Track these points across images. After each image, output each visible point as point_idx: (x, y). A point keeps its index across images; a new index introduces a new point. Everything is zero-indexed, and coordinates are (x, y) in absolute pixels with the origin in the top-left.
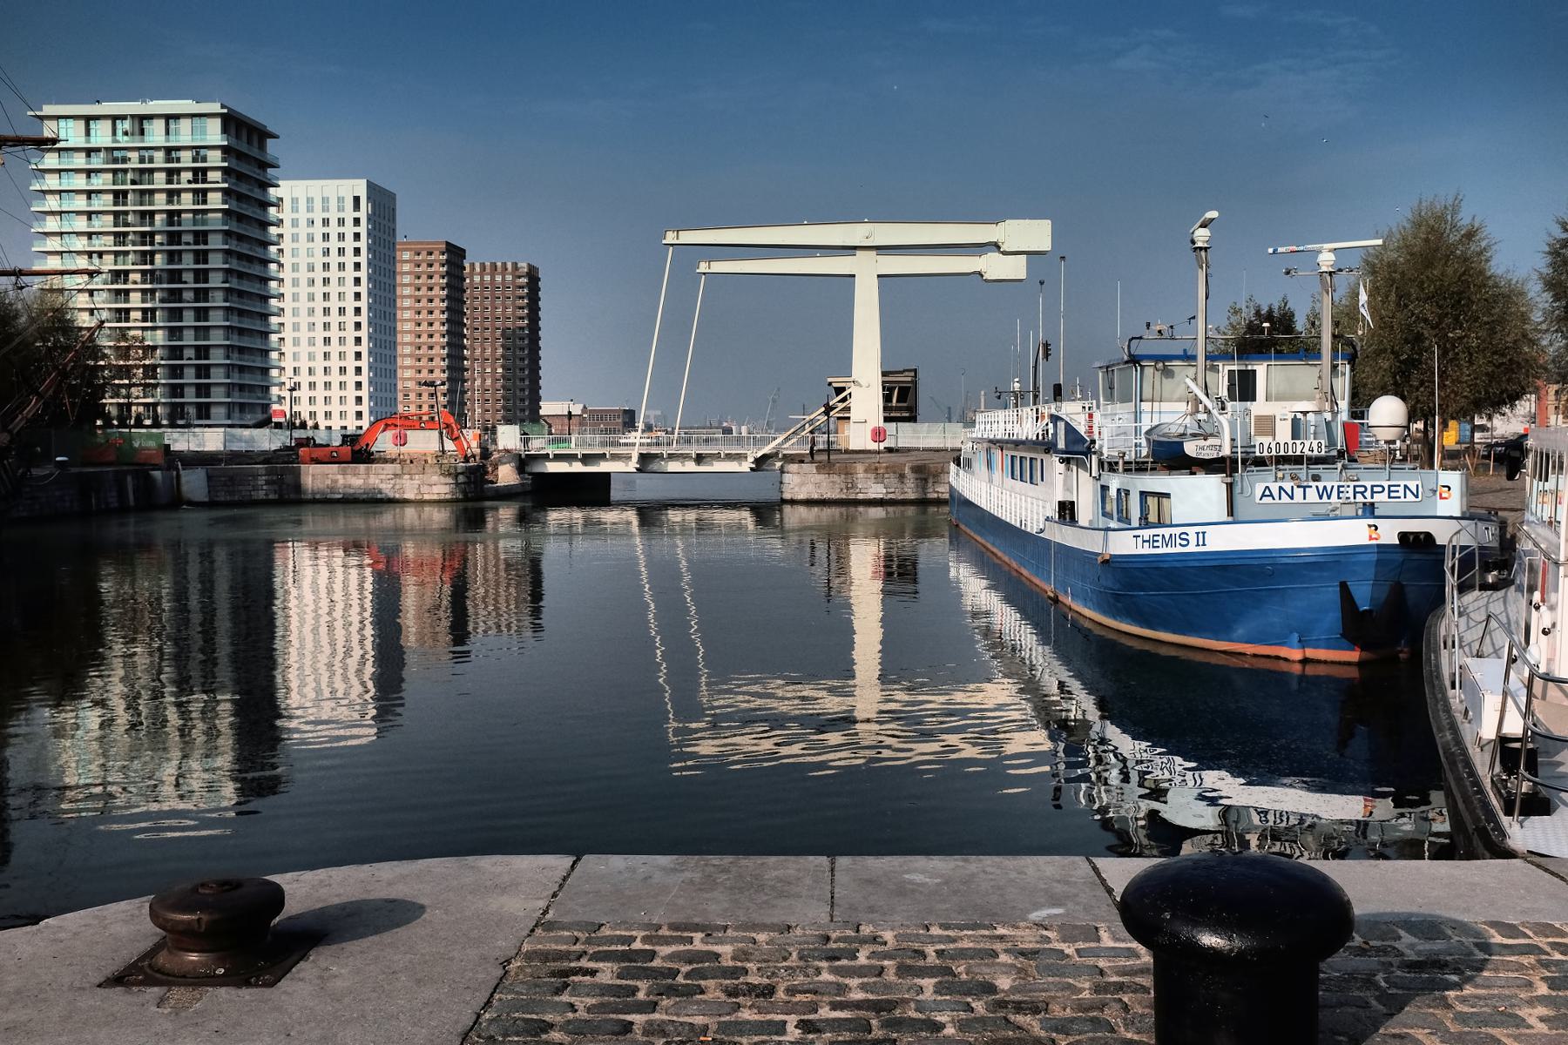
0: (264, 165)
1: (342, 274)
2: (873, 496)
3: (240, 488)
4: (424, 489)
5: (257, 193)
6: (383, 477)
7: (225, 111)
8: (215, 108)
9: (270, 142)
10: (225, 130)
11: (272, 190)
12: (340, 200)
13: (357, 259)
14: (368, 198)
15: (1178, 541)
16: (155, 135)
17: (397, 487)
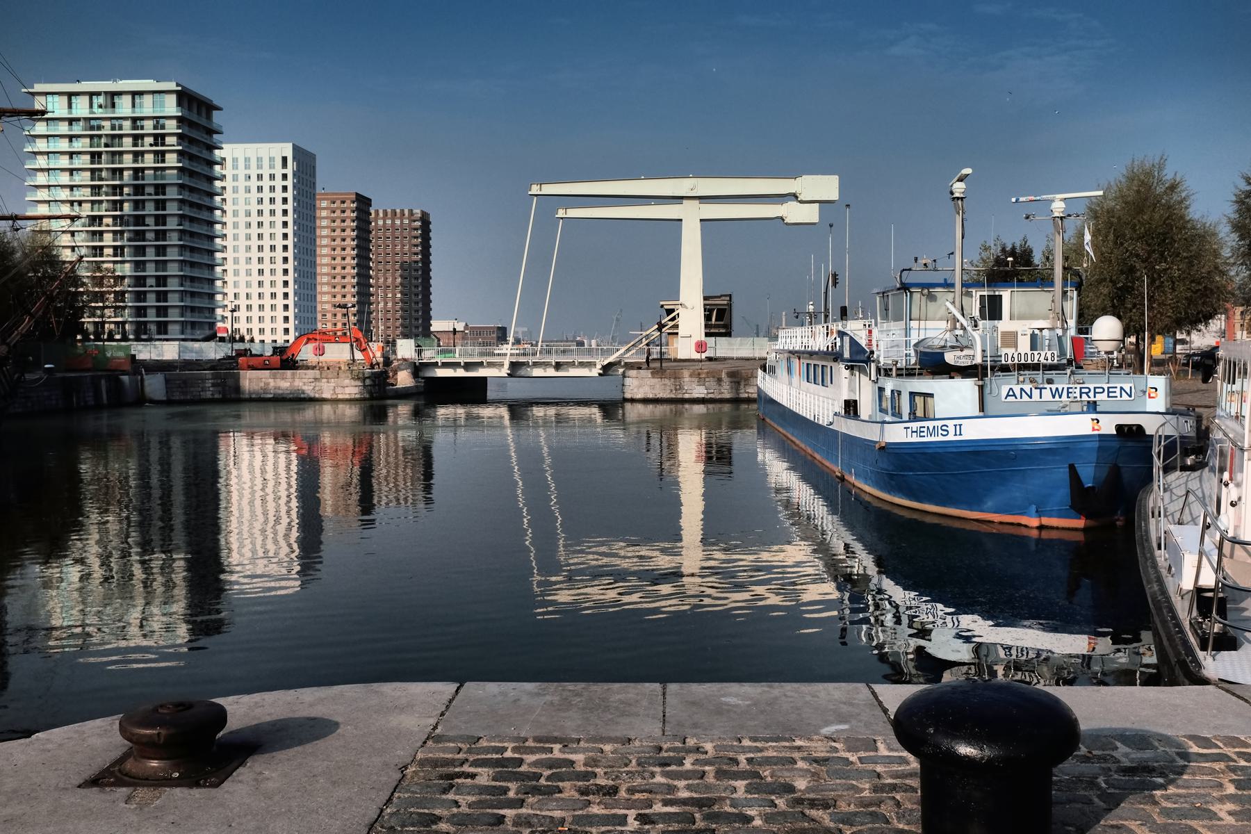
0: (211, 132)
2: (696, 396)
3: (192, 389)
4: (339, 390)
5: (205, 154)
6: (306, 380)
7: (180, 88)
8: (172, 86)
10: (179, 104)
11: (217, 152)
12: (272, 159)
15: (940, 431)
16: (124, 107)
17: (317, 388)
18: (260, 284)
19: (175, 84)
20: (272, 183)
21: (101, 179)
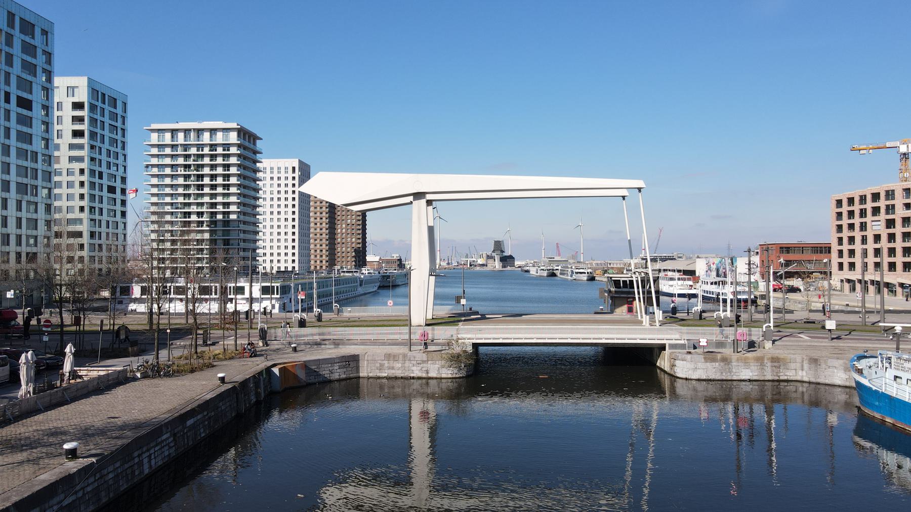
0: (255, 152)
1: (286, 210)
2: (743, 378)
7: (239, 127)
8: (234, 125)
9: (258, 142)
10: (239, 136)
11: (258, 165)
12: (286, 168)
13: (294, 182)
14: (299, 168)
16: (206, 138)
17: (424, 369)
18: (279, 192)
19: (236, 124)
20: (286, 189)
21: (177, 208)
